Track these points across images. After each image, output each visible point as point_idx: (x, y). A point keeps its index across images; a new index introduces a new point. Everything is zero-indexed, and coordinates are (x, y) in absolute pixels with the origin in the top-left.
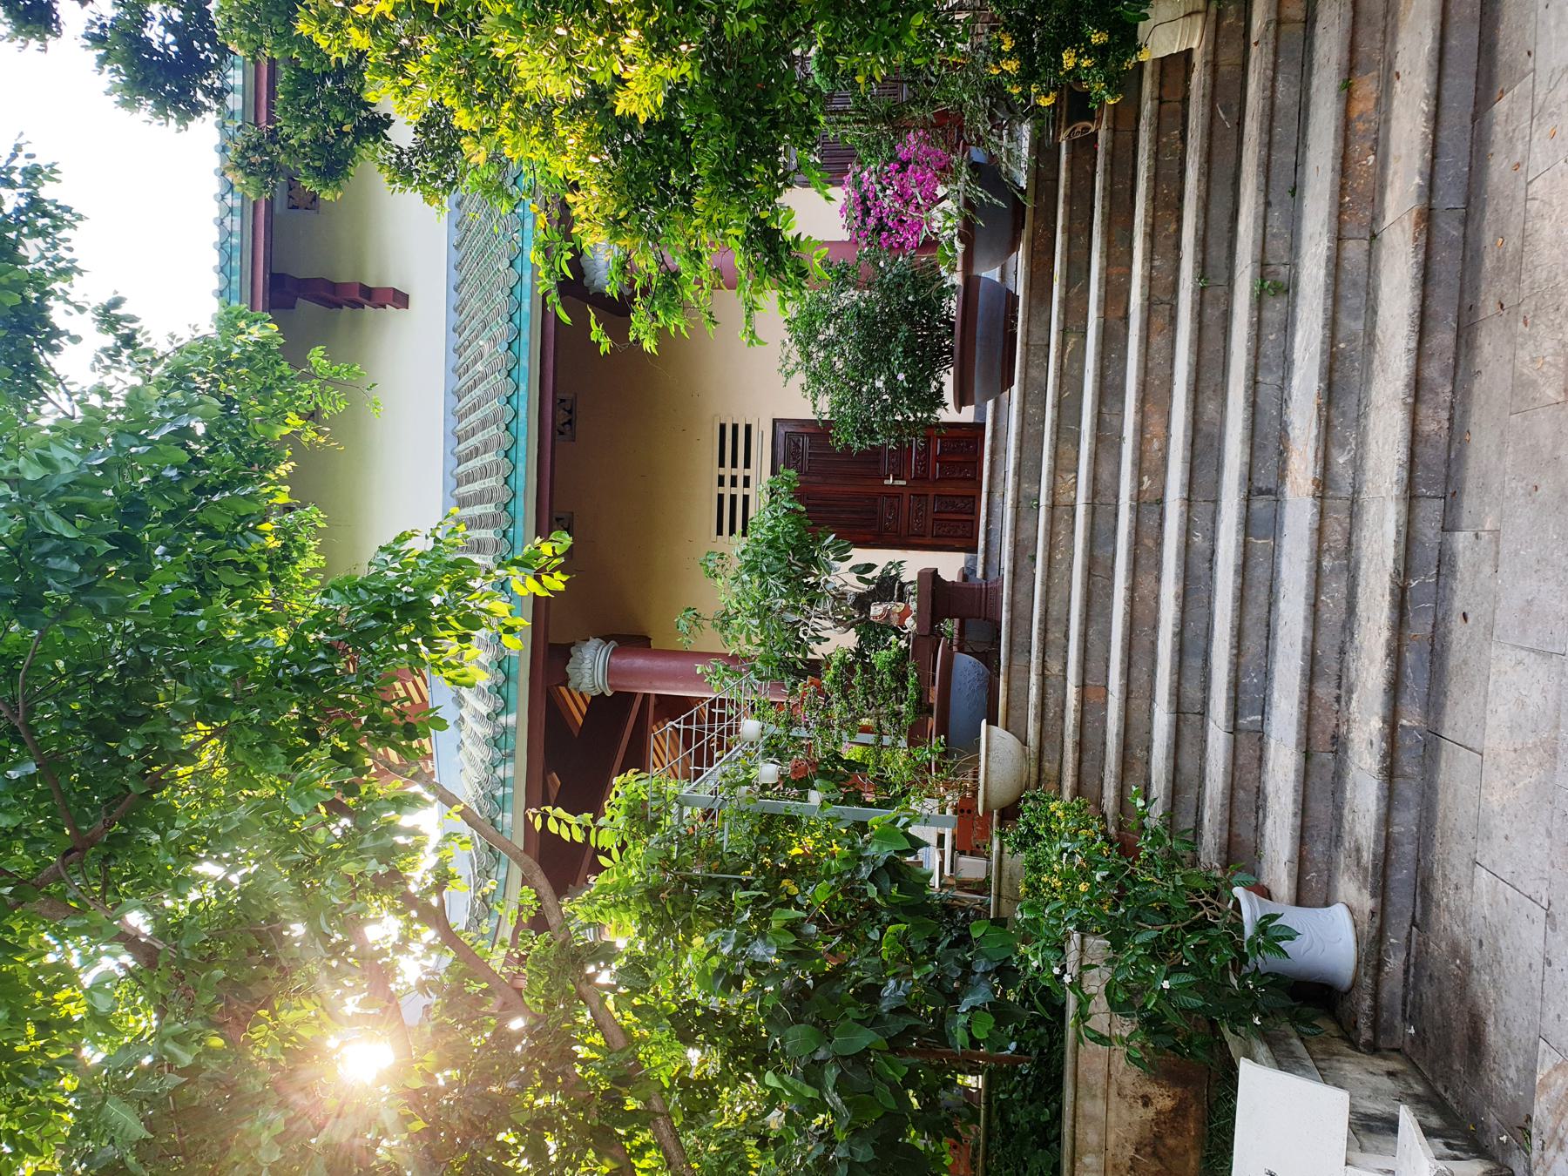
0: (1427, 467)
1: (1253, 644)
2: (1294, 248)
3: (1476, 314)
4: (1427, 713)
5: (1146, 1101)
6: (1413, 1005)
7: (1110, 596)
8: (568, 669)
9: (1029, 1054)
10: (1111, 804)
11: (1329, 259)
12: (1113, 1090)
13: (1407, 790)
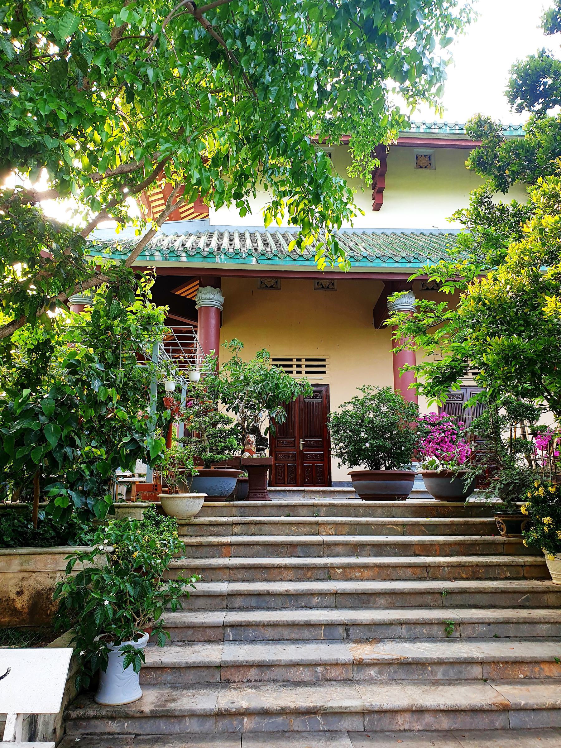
0: (379, 720)
1: (270, 633)
2: (469, 639)
3: (461, 740)
4: (251, 732)
5: (20, 593)
6: (91, 739)
7: (278, 556)
8: (209, 287)
9: (38, 528)
10: (174, 563)
12: (26, 575)
13: (209, 725)
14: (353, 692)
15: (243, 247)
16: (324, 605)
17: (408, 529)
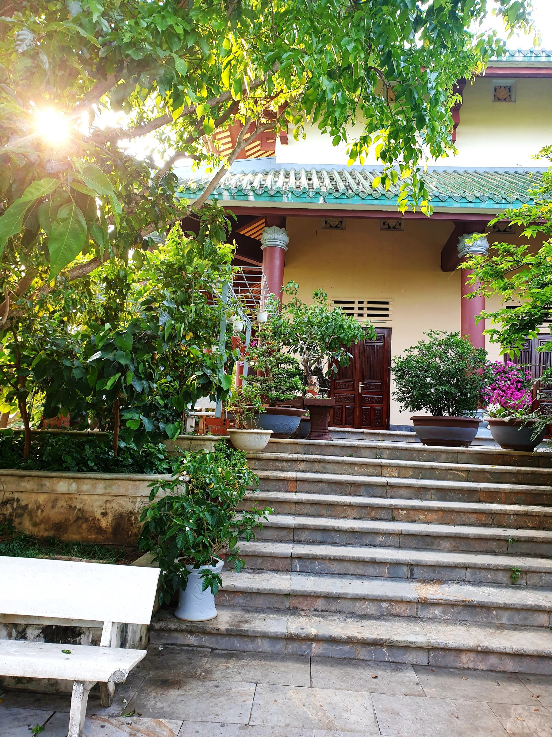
0: (444, 657)
1: (335, 567)
2: (535, 587)
4: (319, 656)
5: (104, 514)
6: (173, 649)
7: (341, 494)
8: (274, 227)
11: (540, 606)
12: (109, 498)
13: (280, 646)
14: (418, 629)
15: (311, 185)
16: (388, 544)
17: (472, 476)
